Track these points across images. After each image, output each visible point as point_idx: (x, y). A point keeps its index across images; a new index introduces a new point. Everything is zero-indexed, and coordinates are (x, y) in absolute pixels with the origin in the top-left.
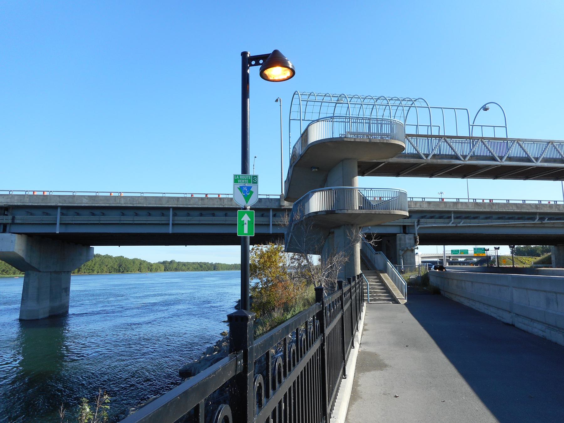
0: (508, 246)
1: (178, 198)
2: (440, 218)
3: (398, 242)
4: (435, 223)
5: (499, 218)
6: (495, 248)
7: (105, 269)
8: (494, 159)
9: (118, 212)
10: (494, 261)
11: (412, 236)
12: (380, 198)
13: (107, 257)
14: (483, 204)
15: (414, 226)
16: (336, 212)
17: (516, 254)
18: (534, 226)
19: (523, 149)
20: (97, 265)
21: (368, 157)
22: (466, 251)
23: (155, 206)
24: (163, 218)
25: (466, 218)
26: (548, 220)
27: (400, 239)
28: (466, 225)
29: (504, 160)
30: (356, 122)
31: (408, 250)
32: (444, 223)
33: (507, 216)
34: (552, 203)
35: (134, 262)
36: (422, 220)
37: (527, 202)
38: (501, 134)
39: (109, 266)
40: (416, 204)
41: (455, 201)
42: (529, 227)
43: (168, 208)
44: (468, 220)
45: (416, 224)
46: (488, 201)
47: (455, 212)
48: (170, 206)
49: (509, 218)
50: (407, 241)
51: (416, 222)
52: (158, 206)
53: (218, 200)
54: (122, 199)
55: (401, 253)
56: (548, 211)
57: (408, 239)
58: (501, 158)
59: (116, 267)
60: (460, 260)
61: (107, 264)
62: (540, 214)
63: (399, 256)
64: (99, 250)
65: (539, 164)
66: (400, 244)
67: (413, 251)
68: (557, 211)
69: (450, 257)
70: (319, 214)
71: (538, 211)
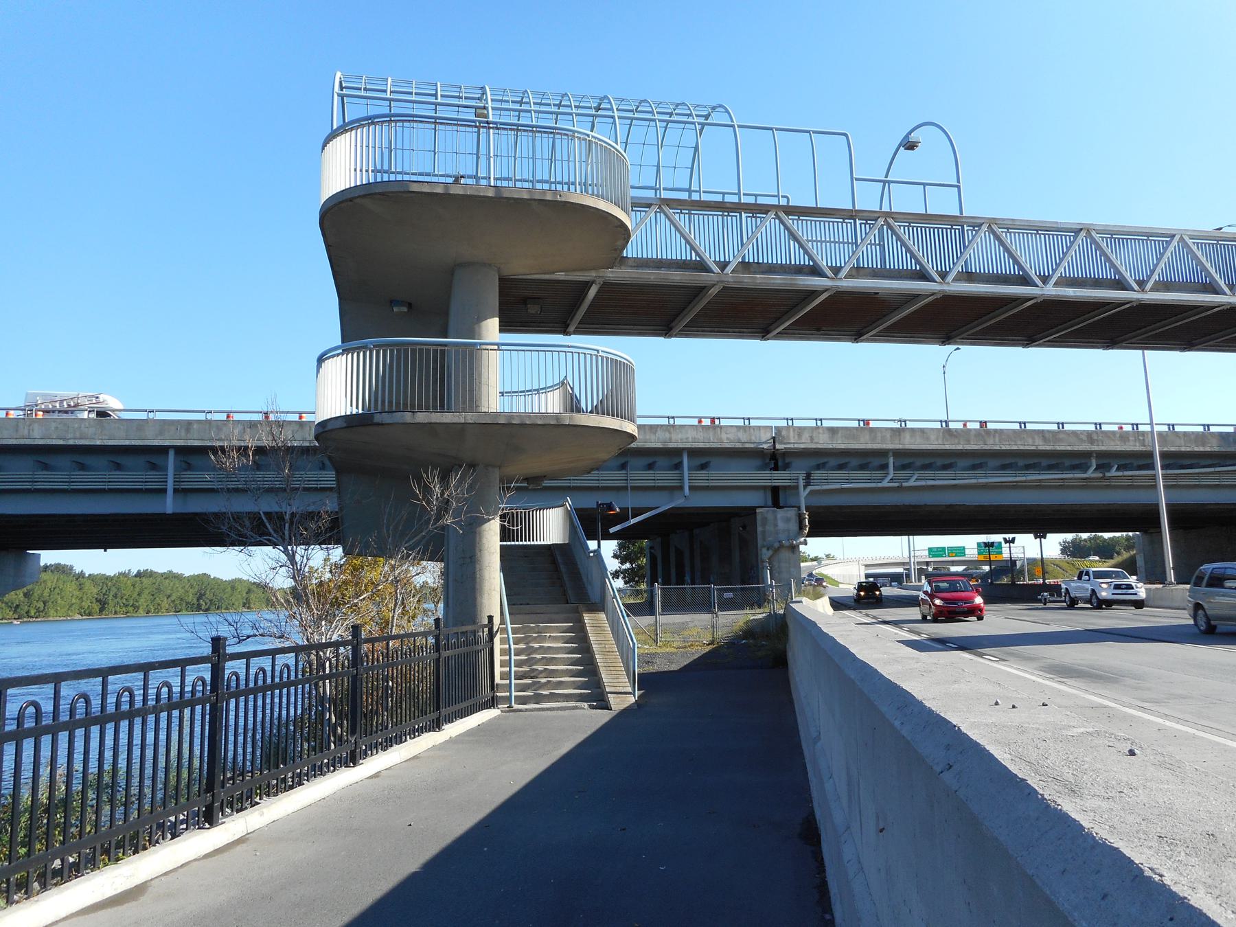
0: (1031, 536)
1: (189, 423)
2: (862, 467)
3: (759, 529)
4: (848, 480)
5: (1003, 467)
6: (1006, 541)
7: (165, 604)
8: (923, 275)
9: (29, 461)
10: (1021, 572)
11: (791, 513)
12: (713, 420)
13: (170, 576)
14: (965, 433)
15: (797, 488)
16: (378, 418)
17: (1073, 555)
18: (1086, 485)
19: (1007, 250)
20: (145, 595)
21: (530, 260)
22: (961, 550)
23: (127, 443)
24: (152, 475)
25: (925, 467)
26: (1118, 469)
27: (765, 520)
28: (923, 483)
29: (950, 278)
30: (556, 183)
31: (781, 546)
32: (870, 480)
33: (1021, 463)
34: (1128, 428)
35: (233, 588)
36: (817, 474)
37: (1067, 427)
38: (942, 204)
39: (173, 598)
40: (800, 435)
41: (897, 425)
42: (1073, 487)
43: (163, 450)
44: (929, 473)
45: (801, 483)
46: (977, 426)
47: (898, 454)
48: (167, 443)
49: (1028, 467)
50: (781, 525)
51: (802, 477)
52: (133, 443)
53: (296, 427)
54: (36, 426)
55: (765, 554)
56: (1119, 448)
57: (782, 520)
58: (943, 275)
59: (191, 598)
60: (954, 569)
61: (169, 592)
62: (1101, 455)
63: (763, 562)
64: (48, 557)
65: (1050, 290)
66: (764, 532)
67: (794, 549)
68: (1138, 448)
69: (927, 563)
70: (329, 427)
71: (1095, 448)
